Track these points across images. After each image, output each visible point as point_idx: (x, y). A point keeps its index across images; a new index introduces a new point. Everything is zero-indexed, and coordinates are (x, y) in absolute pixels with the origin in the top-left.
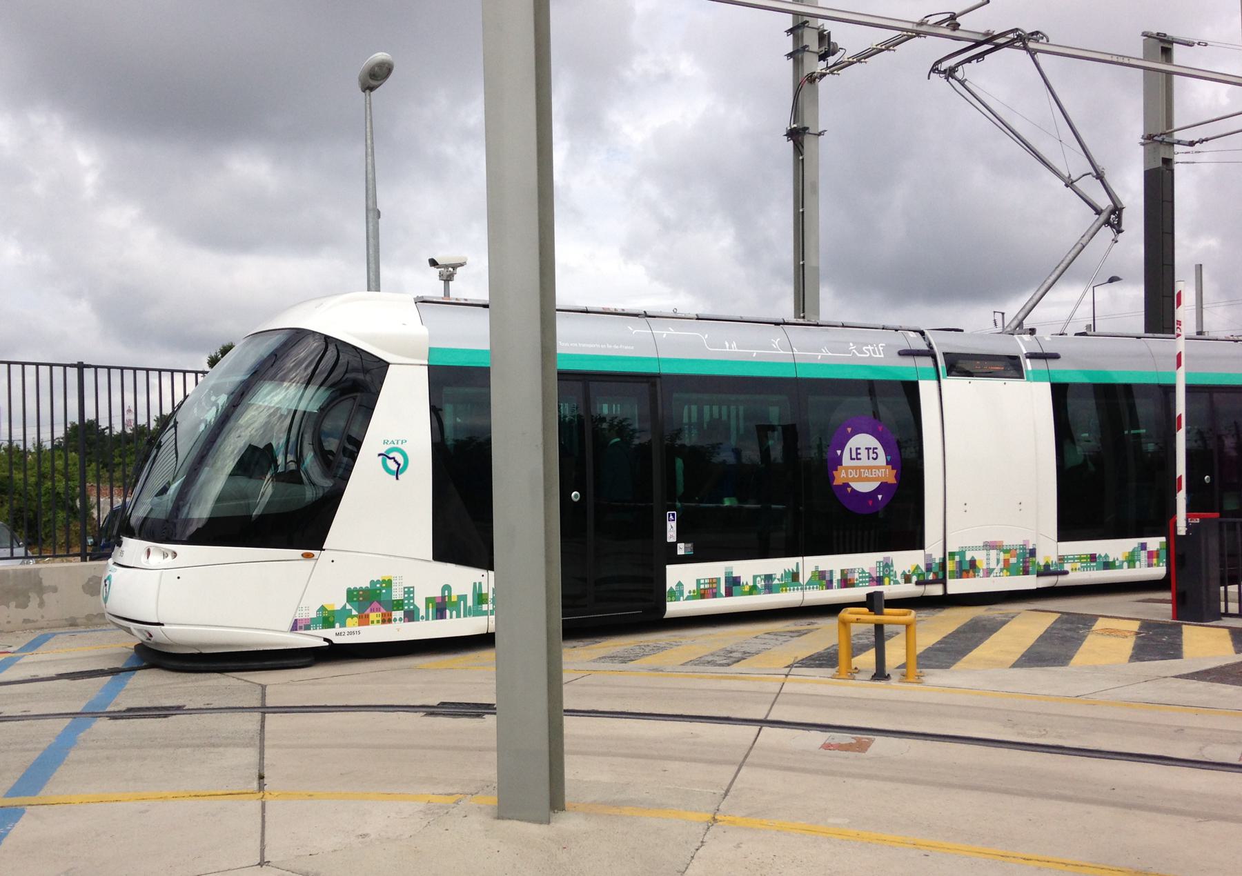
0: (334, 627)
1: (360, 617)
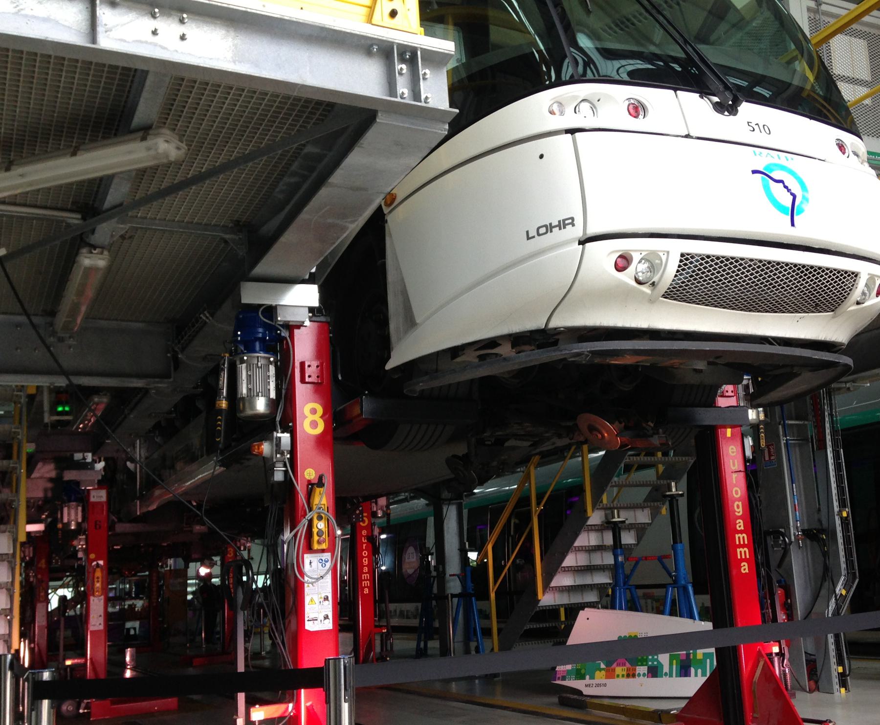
0: (584, 679)
1: (607, 671)
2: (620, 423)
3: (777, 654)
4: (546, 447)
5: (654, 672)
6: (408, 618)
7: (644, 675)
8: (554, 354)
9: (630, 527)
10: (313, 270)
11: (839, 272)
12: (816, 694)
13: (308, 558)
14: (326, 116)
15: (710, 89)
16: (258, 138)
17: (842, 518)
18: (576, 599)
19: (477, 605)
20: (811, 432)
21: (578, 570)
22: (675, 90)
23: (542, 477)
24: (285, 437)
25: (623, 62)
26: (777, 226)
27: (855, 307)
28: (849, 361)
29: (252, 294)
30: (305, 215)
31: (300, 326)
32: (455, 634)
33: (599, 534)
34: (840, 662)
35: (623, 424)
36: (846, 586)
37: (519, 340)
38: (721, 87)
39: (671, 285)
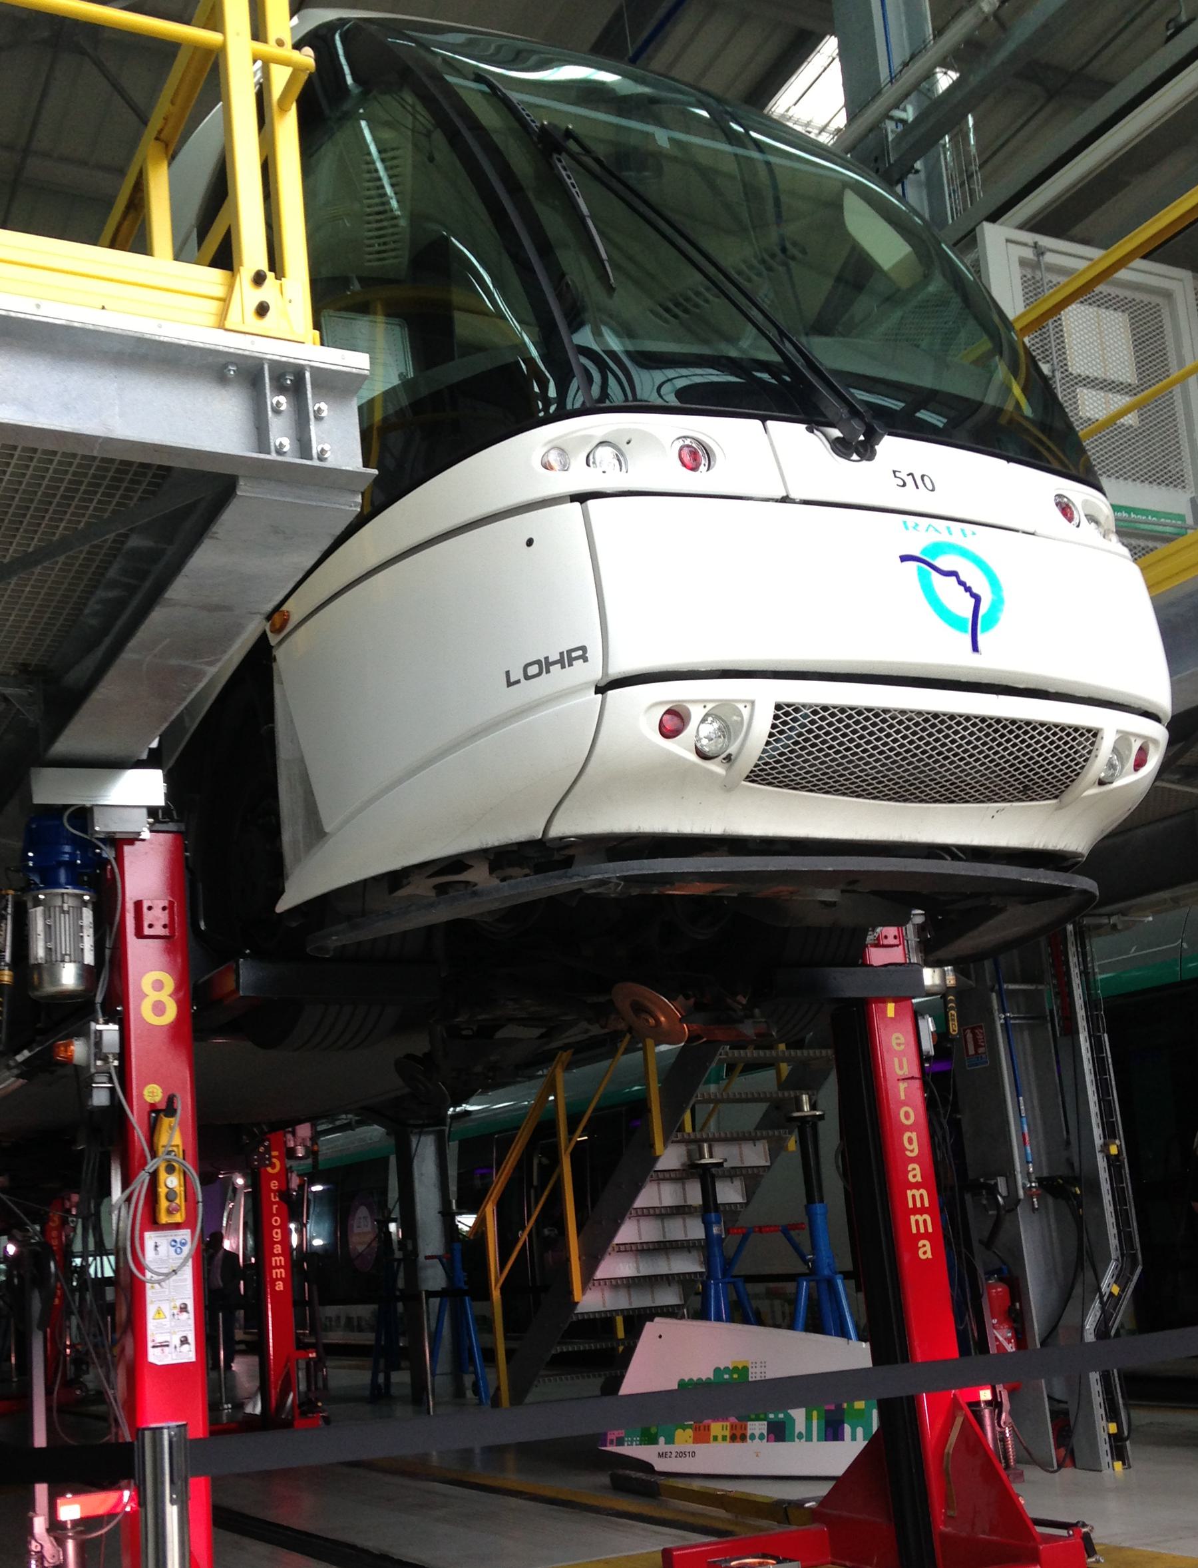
2: (687, 997)
3: (988, 1403)
4: (574, 1035)
5: (779, 1432)
6: (360, 1330)
7: (761, 1437)
8: (559, 883)
9: (732, 1174)
10: (154, 744)
11: (1063, 730)
12: (1068, 1473)
13: (150, 1238)
14: (158, 485)
15: (824, 416)
16: (47, 526)
17: (1109, 1157)
18: (641, 1300)
19: (472, 1308)
20: (1050, 1003)
21: (643, 1250)
22: (763, 419)
23: (569, 1087)
24: (110, 1031)
25: (671, 373)
26: (949, 652)
27: (1096, 790)
28: (1089, 884)
29: (51, 789)
30: (129, 655)
31: (133, 839)
32: (436, 1362)
33: (678, 1186)
34: (1112, 1414)
35: (692, 1000)
36: (1121, 1279)
37: (503, 858)
38: (844, 412)
39: (760, 758)
